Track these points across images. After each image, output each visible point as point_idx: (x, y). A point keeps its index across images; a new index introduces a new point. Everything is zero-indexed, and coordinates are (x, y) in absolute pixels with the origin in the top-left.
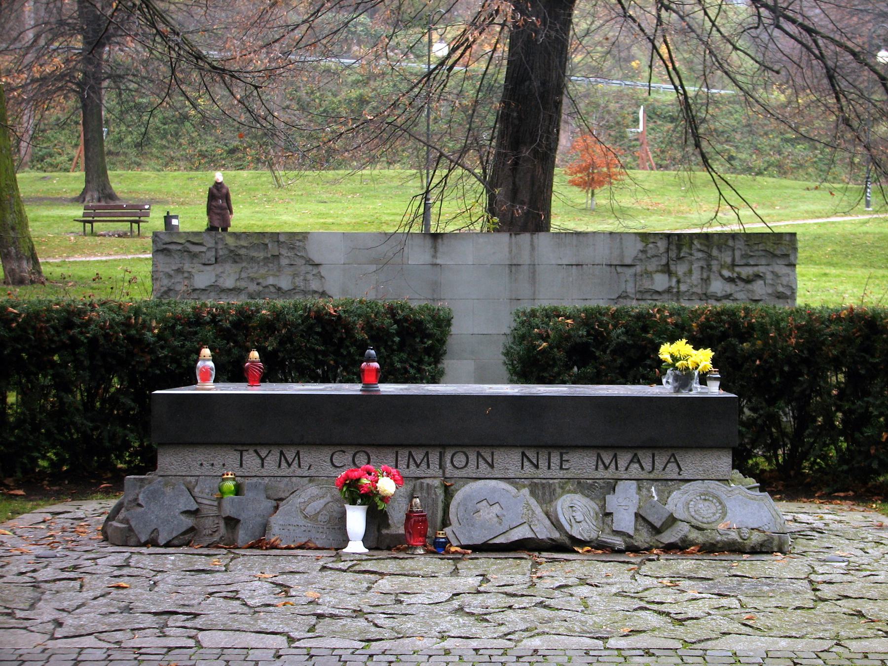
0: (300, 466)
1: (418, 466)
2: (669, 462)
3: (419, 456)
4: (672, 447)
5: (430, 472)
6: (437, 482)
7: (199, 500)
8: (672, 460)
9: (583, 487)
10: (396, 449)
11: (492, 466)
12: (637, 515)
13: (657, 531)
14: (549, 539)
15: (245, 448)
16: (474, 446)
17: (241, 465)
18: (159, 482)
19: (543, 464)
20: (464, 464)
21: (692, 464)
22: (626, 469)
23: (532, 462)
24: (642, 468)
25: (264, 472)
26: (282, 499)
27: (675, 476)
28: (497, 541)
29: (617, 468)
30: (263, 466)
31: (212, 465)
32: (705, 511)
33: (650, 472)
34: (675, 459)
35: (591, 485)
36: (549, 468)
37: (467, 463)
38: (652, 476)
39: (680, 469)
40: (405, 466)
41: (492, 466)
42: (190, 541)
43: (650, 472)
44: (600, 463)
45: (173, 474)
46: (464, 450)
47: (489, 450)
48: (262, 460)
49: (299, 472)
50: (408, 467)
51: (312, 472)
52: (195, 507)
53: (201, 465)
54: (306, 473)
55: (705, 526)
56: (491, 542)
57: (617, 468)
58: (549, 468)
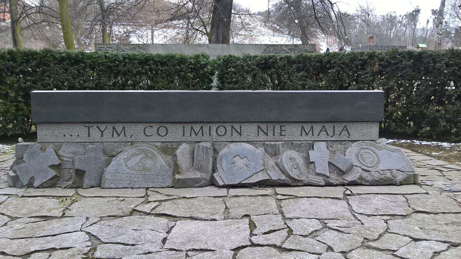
0: (125, 136)
1: (196, 135)
2: (321, 131)
3: (197, 128)
4: (201, 122)
5: (204, 138)
6: (209, 145)
7: (62, 158)
8: (345, 129)
9: (291, 145)
10: (183, 125)
11: (240, 134)
12: (330, 164)
13: (342, 173)
14: (279, 179)
15: (91, 125)
16: (265, 122)
17: (89, 136)
18: (37, 147)
19: (270, 133)
20: (224, 133)
21: (356, 130)
22: (318, 135)
23: (264, 132)
24: (328, 135)
25: (91, 139)
26: (114, 156)
27: (346, 138)
28: (246, 181)
29: (313, 135)
30: (102, 136)
31: (71, 135)
32: (369, 159)
33: (332, 137)
34: (346, 128)
35: (300, 145)
36: (274, 135)
37: (226, 133)
38: (333, 139)
39: (350, 135)
40: (189, 135)
41: (240, 134)
42: (55, 184)
43: (332, 137)
44: (303, 131)
45: (48, 141)
46: (224, 125)
47: (331, 125)
48: (102, 132)
49: (124, 139)
50: (191, 136)
51: (133, 139)
52: (57, 162)
53: (64, 135)
54: (129, 140)
55: (369, 169)
56: (243, 182)
57: (313, 135)
58: (274, 135)
